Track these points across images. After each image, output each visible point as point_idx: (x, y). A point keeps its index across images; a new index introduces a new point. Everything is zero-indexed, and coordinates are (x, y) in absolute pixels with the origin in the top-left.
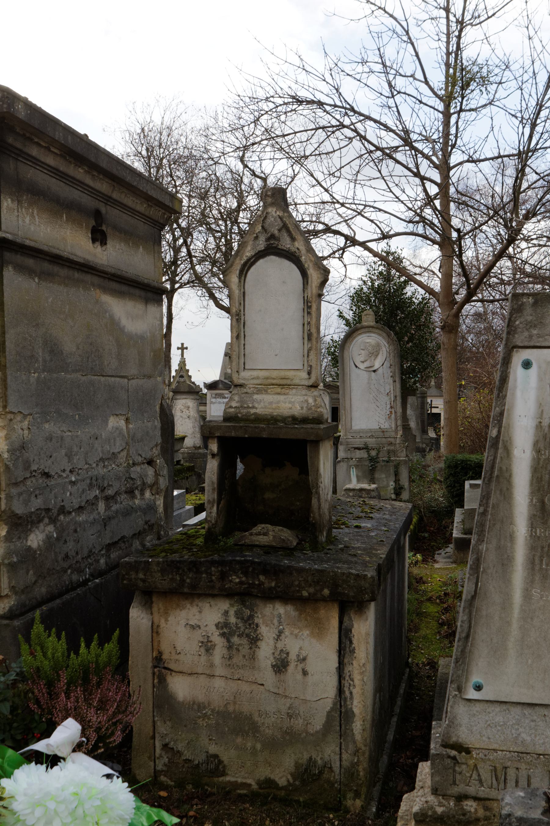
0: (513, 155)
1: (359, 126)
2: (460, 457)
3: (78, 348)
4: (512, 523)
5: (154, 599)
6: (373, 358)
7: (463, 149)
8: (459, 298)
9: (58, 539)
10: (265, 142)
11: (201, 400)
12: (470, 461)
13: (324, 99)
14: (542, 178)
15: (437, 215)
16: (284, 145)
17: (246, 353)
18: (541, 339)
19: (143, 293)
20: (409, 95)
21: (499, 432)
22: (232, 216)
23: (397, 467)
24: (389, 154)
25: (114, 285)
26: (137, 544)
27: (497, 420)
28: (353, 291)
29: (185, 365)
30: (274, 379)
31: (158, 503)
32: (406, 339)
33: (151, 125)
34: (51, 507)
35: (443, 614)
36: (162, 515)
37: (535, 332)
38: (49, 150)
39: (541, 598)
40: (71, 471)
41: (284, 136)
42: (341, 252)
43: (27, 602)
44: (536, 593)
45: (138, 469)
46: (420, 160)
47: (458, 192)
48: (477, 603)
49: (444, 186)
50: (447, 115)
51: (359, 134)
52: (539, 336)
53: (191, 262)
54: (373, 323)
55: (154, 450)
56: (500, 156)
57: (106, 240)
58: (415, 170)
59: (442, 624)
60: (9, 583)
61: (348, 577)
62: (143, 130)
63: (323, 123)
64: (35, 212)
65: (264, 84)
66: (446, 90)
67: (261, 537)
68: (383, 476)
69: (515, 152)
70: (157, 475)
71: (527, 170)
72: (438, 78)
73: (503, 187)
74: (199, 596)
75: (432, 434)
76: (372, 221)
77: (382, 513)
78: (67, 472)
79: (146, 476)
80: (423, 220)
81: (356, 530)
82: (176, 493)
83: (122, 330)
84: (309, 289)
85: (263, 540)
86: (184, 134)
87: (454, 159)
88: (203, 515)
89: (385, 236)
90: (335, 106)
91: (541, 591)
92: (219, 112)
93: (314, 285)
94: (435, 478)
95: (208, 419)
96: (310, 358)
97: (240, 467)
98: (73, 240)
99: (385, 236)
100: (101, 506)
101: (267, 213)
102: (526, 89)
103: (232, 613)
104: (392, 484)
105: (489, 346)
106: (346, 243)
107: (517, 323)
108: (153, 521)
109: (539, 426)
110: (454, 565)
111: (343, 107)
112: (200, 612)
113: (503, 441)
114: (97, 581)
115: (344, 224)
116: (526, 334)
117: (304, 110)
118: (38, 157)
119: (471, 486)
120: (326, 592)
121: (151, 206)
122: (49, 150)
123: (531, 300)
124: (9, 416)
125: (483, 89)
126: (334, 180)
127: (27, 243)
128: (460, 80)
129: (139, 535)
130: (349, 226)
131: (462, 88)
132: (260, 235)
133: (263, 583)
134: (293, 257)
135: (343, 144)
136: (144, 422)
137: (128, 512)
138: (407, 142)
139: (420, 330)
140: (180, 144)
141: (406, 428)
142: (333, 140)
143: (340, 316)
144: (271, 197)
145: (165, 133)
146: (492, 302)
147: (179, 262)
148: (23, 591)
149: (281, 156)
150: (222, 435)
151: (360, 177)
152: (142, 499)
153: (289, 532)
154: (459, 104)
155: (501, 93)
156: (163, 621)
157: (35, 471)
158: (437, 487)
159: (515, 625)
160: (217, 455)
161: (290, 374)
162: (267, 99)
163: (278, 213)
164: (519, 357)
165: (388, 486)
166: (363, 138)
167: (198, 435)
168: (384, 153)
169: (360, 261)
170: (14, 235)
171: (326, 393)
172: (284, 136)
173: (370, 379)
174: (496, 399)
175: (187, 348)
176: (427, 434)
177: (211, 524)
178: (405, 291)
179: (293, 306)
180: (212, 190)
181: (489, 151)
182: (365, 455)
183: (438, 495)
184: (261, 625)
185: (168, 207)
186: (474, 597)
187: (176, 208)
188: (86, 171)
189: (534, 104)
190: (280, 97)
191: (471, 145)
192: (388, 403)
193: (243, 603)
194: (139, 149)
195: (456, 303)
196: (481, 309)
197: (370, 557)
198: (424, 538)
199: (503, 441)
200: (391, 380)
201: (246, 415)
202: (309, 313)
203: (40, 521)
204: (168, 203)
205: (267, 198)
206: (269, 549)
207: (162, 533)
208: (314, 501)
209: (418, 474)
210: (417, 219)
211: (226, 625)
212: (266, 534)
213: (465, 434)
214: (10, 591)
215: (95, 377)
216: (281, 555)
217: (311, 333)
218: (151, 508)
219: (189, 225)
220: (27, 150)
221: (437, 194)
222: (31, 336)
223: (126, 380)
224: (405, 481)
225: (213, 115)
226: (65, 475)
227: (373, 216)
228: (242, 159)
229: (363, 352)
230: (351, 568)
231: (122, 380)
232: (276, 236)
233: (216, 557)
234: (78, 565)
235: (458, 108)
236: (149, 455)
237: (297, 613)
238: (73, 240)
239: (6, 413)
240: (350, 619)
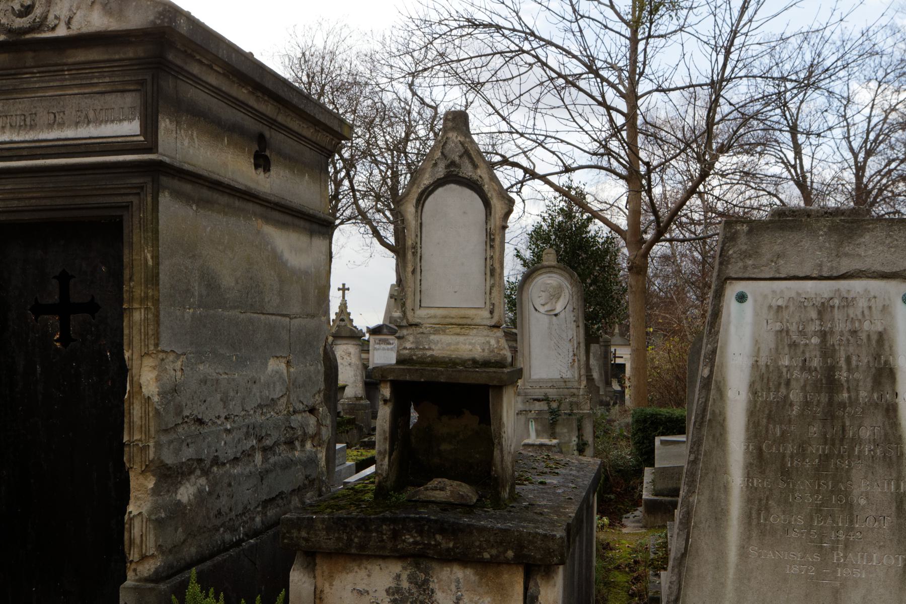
0: (706, 85)
1: (540, 52)
2: (649, 410)
3: (237, 283)
4: (725, 473)
5: (317, 561)
6: (554, 300)
7: (652, 77)
8: (648, 237)
9: (210, 493)
10: (438, 67)
11: (364, 347)
13: (502, 23)
14: (737, 109)
15: (624, 147)
16: (460, 70)
18: (756, 270)
19: (307, 225)
20: (593, 19)
21: (711, 372)
22: (399, 147)
23: (580, 421)
24: (571, 81)
25: (276, 215)
26: (295, 501)
27: (709, 358)
28: (532, 229)
29: (346, 307)
31: (319, 455)
32: (588, 281)
33: (313, 50)
34: (203, 457)
35: (634, 584)
36: (324, 469)
37: (750, 262)
38: (212, 68)
39: (759, 556)
40: (226, 418)
41: (459, 61)
42: (519, 185)
43: (175, 563)
44: (753, 550)
45: (299, 417)
46: (605, 88)
47: (646, 123)
48: (688, 561)
49: (631, 117)
50: (634, 41)
51: (539, 60)
52: (755, 267)
53: (354, 196)
54: (554, 263)
56: (693, 86)
57: (270, 166)
58: (600, 99)
59: (632, 596)
60: (156, 541)
61: (534, 537)
62: (304, 54)
63: (501, 48)
64: (195, 134)
65: (438, 7)
66: (633, 15)
67: (437, 492)
68: (565, 430)
69: (708, 81)
70: (319, 424)
71: (721, 100)
73: (696, 117)
74: (369, 557)
75: (616, 387)
76: (553, 153)
77: (568, 468)
78: (222, 419)
79: (308, 425)
80: (609, 153)
81: (541, 486)
82: (338, 446)
83: (284, 264)
84: (492, 220)
85: (440, 496)
86: (349, 59)
87: (642, 88)
88: (371, 469)
89: (568, 169)
90: (514, 30)
91: (759, 549)
92: (386, 36)
93: (497, 216)
94: (621, 434)
95: (371, 367)
96: (493, 295)
97: (414, 416)
98: (234, 165)
99: (568, 169)
100: (258, 457)
102: (719, 15)
103: (404, 577)
104: (575, 439)
105: (680, 291)
106: (525, 176)
107: (731, 252)
108: (314, 476)
109: (755, 365)
110: (644, 530)
111: (523, 32)
112: (369, 576)
113: (716, 381)
114: (252, 541)
115: (523, 155)
116: (740, 264)
117: (479, 33)
118: (199, 76)
119: (662, 442)
120: (510, 554)
122: (212, 68)
123: (745, 228)
124: (161, 355)
125: (673, 14)
126: (512, 109)
127: (186, 167)
129: (298, 491)
130: (528, 158)
131: (651, 13)
132: (439, 161)
133: (440, 544)
135: (523, 70)
137: (288, 465)
138: (592, 69)
139: (605, 271)
140: (344, 70)
141: (590, 379)
142: (513, 67)
143: (517, 256)
145: (327, 58)
146: (683, 241)
147: (341, 197)
148: (170, 551)
149: (455, 82)
151: (540, 105)
152: (303, 451)
153: (468, 487)
154: (647, 30)
155: (692, 19)
156: (327, 585)
157: (187, 417)
158: (624, 443)
159: (730, 586)
160: (390, 400)
161: (471, 313)
162: (440, 23)
163: (459, 138)
164: (733, 290)
165: (570, 441)
166: (544, 64)
167: (360, 385)
168: (567, 82)
169: (539, 196)
170: (172, 158)
172: (459, 61)
173: (550, 323)
174: (707, 336)
175: (348, 289)
176: (611, 386)
178: (588, 229)
179: (475, 240)
180: (377, 120)
181: (679, 80)
182: (546, 408)
183: (625, 453)
184: (437, 591)
185: (337, 132)
186: (684, 555)
188: (250, 92)
189: (729, 30)
190: (455, 20)
191: (660, 74)
192: (571, 350)
193: (417, 566)
194: (300, 75)
195: (645, 242)
196: (669, 251)
197: (557, 515)
198: (611, 500)
199: (716, 381)
200: (574, 325)
203: (191, 472)
204: (336, 128)
206: (446, 506)
207: (324, 489)
208: (496, 453)
209: (603, 429)
210: (602, 151)
211: (398, 590)
212: (443, 489)
213: (654, 386)
214: (157, 550)
215: (255, 315)
216: (460, 512)
217: (494, 269)
218: (312, 461)
219: (352, 156)
220: (187, 67)
221: (624, 125)
222: (186, 268)
223: (288, 319)
224: (589, 437)
225: (381, 39)
226: (219, 422)
227: (555, 147)
228: (411, 86)
229: (543, 294)
230: (538, 528)
231: (283, 319)
232: (458, 164)
233: (388, 514)
234: (231, 523)
235: (646, 34)
236: (311, 402)
237: (477, 577)
238: (234, 165)
239: (158, 351)
240: (537, 585)
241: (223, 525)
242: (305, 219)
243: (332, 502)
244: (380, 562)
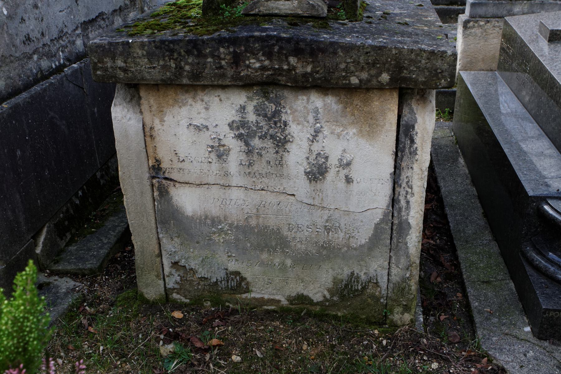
5: (142, 93)
9: (10, 17)
61: (417, 55)
74: (204, 87)
103: (250, 109)
112: (207, 109)
114: (75, 65)
120: (385, 77)
133: (294, 68)
193: (266, 95)
211: (243, 124)
233: (224, 33)
234: (47, 49)
237: (340, 106)
240: (412, 111)
241: (35, 51)
243: (152, 21)
244: (219, 92)
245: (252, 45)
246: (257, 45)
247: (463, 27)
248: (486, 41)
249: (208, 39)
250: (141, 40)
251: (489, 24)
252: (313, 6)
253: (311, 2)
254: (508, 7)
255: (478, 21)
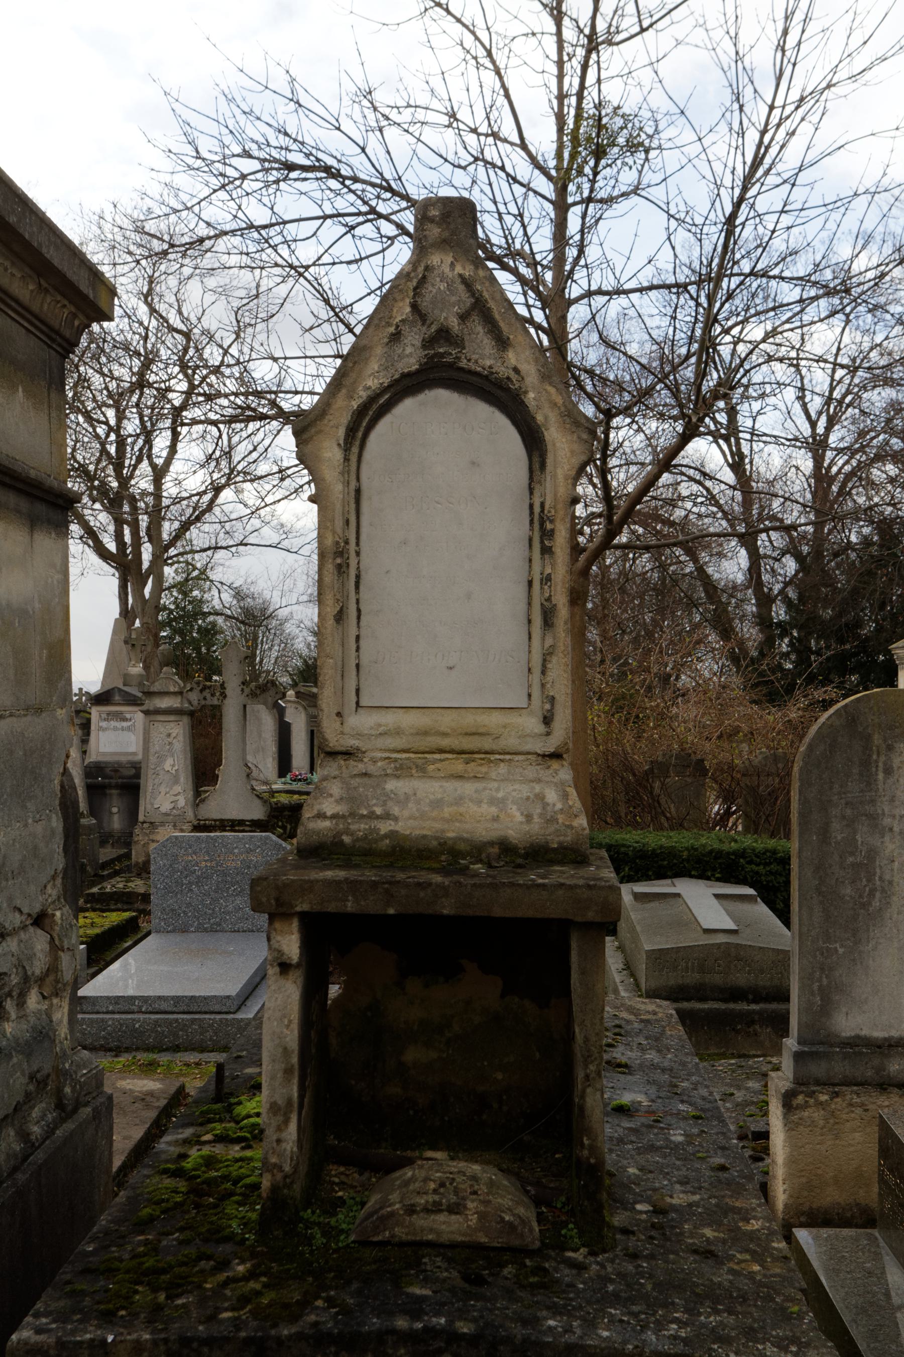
12: (624, 846)
17: (364, 661)
19: (24, 504)
30: (445, 735)
31: (56, 1016)
55: (49, 890)
67: (442, 1217)
70: (55, 948)
72: (544, 138)
84: (549, 484)
93: (560, 473)
96: (551, 675)
101: (427, 268)
108: (47, 1068)
119: (637, 897)
121: (46, 291)
128: (591, 143)
132: (405, 329)
134: (502, 395)
136: (26, 825)
144: (439, 224)
150: (317, 908)
160: (298, 965)
161: (494, 720)
163: (459, 269)
171: (300, 708)
177: (279, 1176)
185: (85, 297)
187: (103, 304)
201: (365, 837)
202: (546, 551)
204: (84, 287)
205: (428, 226)
242: (19, 491)
245: (390, 1351)
246: (402, 1351)
247: (784, 1106)
248: (837, 1137)
249: (290, 1337)
250: (134, 1336)
251: (839, 1100)
252: (511, 1227)
253: (507, 1218)
254: (876, 1062)
255: (814, 1092)
